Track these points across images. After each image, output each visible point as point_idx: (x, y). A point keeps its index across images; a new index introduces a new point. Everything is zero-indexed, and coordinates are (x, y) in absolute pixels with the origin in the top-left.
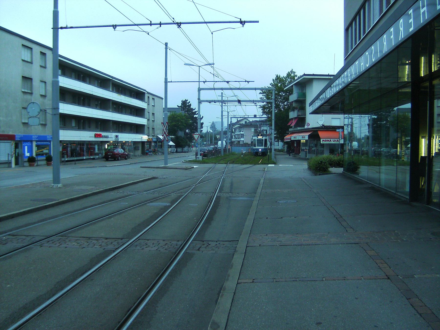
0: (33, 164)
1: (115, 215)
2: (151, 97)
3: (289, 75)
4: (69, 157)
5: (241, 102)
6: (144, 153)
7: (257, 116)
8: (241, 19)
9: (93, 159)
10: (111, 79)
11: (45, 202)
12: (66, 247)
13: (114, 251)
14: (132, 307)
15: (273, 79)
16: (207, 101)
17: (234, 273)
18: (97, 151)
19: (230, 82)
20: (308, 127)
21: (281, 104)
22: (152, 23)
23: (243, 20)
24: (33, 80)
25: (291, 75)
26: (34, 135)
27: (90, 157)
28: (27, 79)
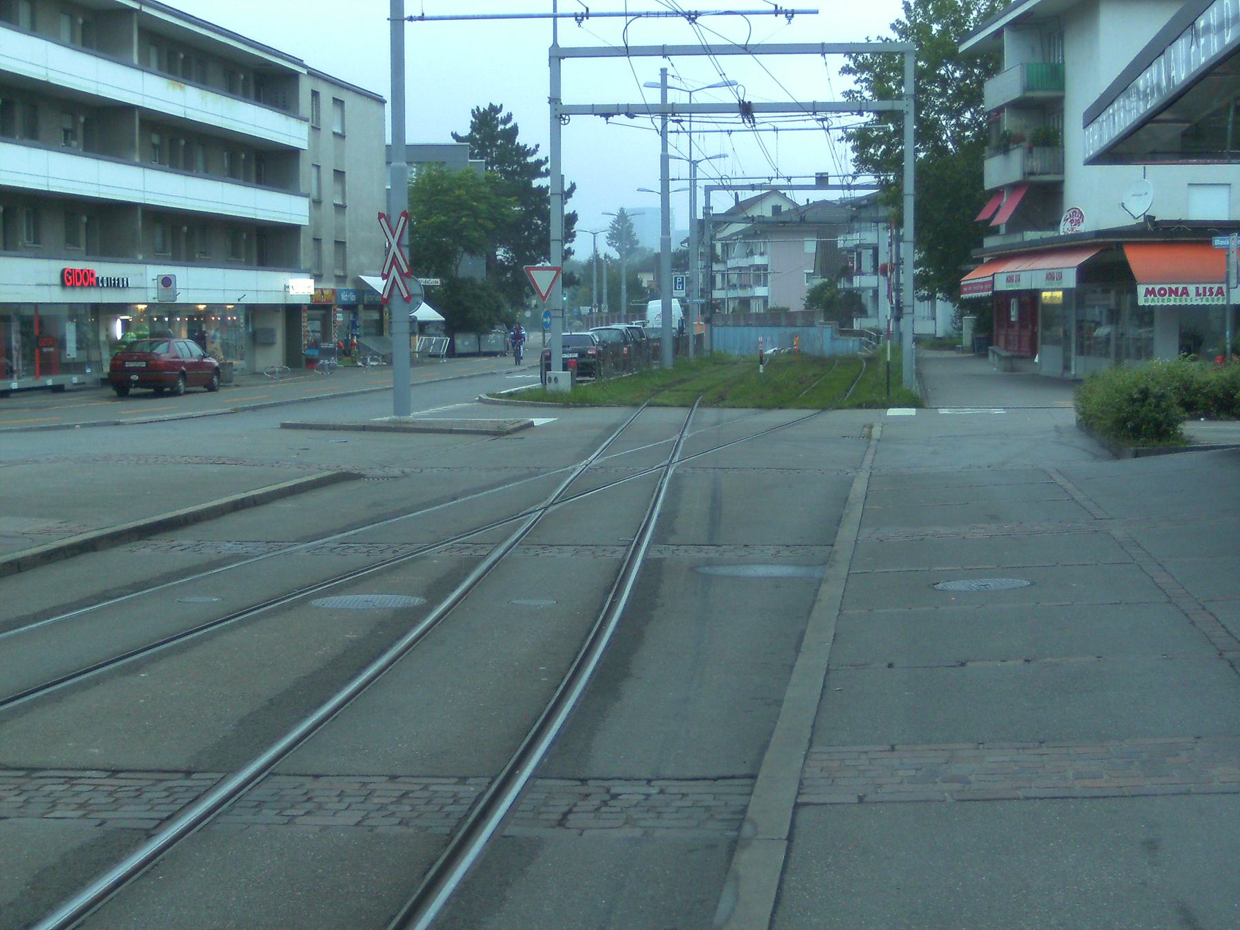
2: (326, 93)
5: (755, 115)
7: (831, 181)
9: (57, 389)
13: (149, 835)
16: (593, 110)
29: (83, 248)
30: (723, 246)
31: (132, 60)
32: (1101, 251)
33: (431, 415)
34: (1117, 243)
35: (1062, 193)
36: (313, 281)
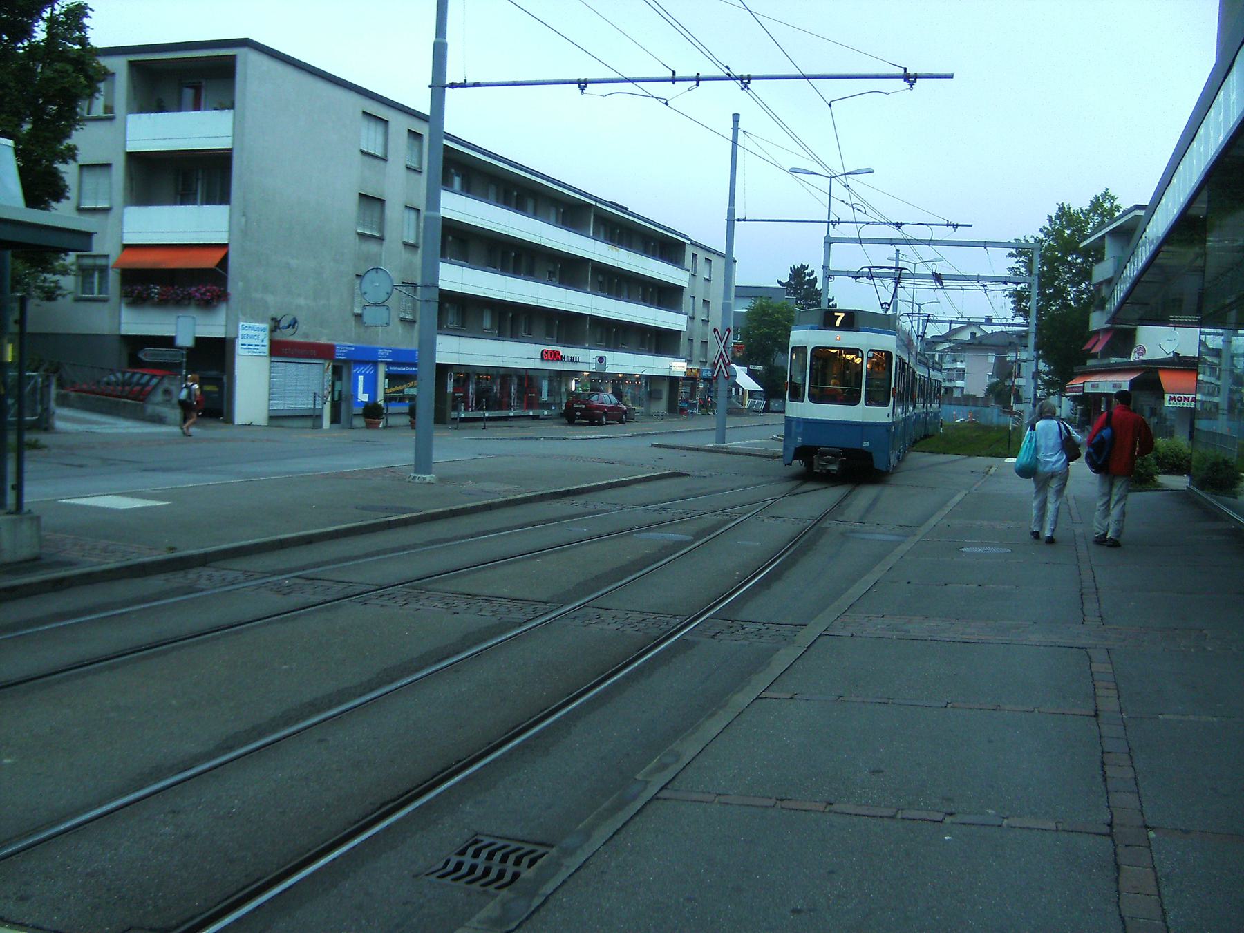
0: (376, 424)
1: (550, 553)
2: (702, 255)
3: (1096, 205)
4: (470, 410)
5: (943, 281)
6: (675, 409)
7: (994, 321)
8: (905, 69)
9: (535, 417)
10: (594, 203)
11: (385, 515)
12: (417, 610)
13: (521, 625)
14: (522, 723)
15: (1049, 216)
16: (848, 274)
17: (760, 682)
18: (545, 397)
19: (903, 224)
20: (1141, 357)
21: (1069, 289)
22: (677, 75)
23: (911, 71)
24: (387, 204)
25: (1101, 206)
26: (382, 346)
27: (527, 411)
28: (371, 202)
29: (555, 339)
30: (939, 355)
31: (590, 233)
32: (1145, 372)
33: (745, 445)
34: (1154, 368)
35: (1135, 335)
36: (686, 363)
